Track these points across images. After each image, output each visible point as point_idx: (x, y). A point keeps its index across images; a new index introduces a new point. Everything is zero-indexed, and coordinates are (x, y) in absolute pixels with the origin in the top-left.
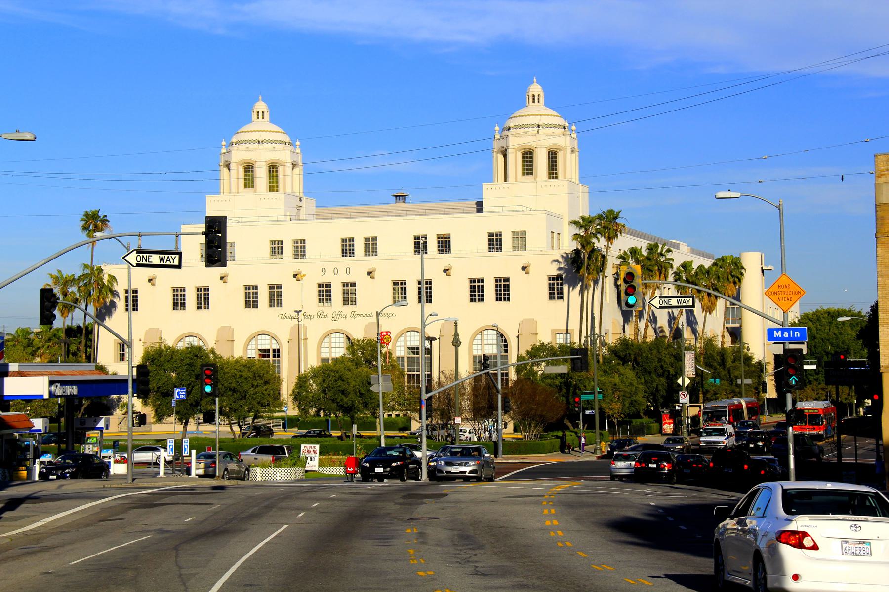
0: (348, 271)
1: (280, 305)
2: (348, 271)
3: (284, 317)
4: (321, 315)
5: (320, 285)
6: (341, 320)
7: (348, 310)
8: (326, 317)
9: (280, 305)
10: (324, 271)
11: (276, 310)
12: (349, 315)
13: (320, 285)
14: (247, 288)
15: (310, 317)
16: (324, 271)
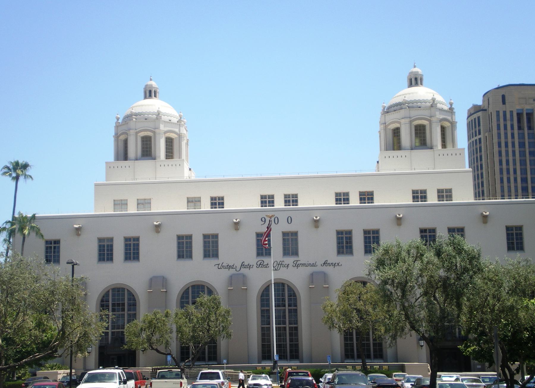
0: (289, 220)
2: (289, 220)
3: (221, 267)
4: (261, 265)
6: (283, 269)
7: (290, 260)
8: (267, 266)
9: (216, 255)
11: (212, 262)
12: (291, 264)
14: (179, 237)
15: (249, 267)
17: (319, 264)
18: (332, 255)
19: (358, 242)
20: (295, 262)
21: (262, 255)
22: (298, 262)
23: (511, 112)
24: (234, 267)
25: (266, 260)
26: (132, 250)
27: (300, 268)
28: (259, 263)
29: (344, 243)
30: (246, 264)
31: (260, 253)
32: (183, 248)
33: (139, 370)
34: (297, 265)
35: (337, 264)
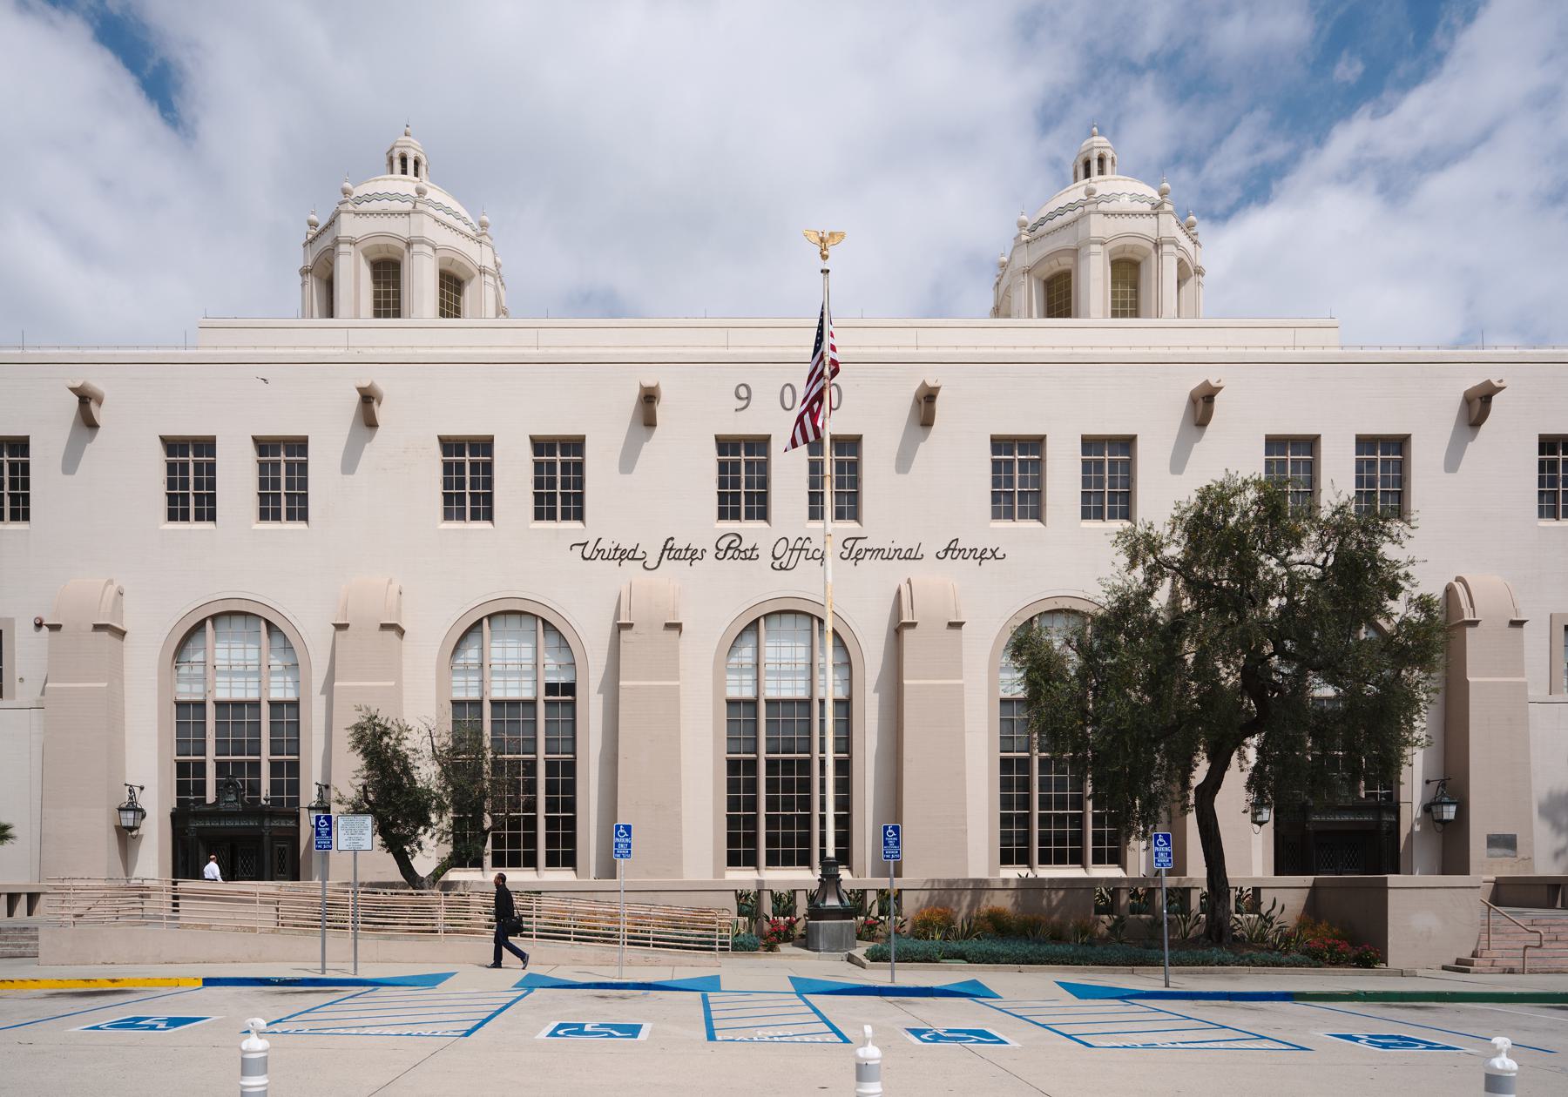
1: (575, 511)
3: (592, 552)
4: (733, 550)
5: (726, 445)
7: (833, 529)
8: (750, 555)
9: (575, 511)
10: (744, 395)
13: (726, 445)
16: (744, 395)
17: (929, 550)
18: (699, 518)
19: (1064, 476)
20: (849, 544)
21: (736, 516)
22: (860, 545)
23: (404, 172)
24: (639, 555)
25: (750, 529)
26: (561, 478)
27: (866, 563)
28: (723, 545)
29: (1016, 472)
30: (679, 544)
31: (728, 508)
32: (185, 485)
33: (275, 823)
34: (854, 552)
35: (989, 554)
